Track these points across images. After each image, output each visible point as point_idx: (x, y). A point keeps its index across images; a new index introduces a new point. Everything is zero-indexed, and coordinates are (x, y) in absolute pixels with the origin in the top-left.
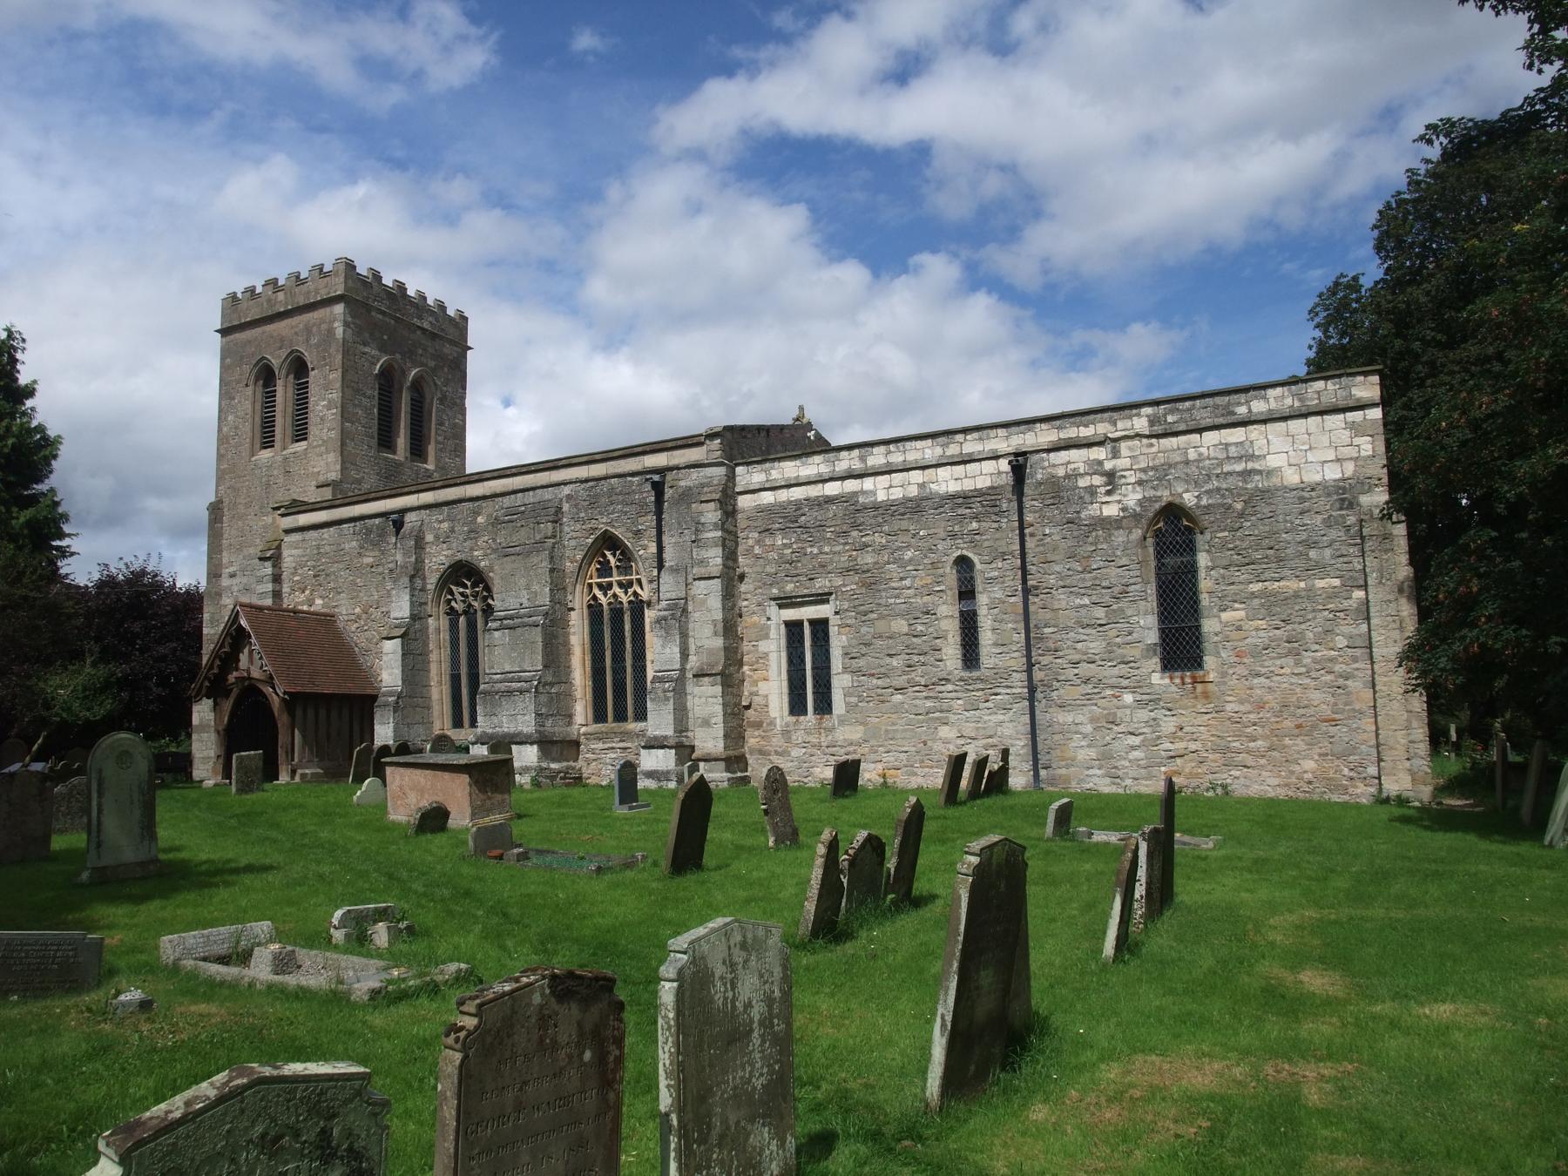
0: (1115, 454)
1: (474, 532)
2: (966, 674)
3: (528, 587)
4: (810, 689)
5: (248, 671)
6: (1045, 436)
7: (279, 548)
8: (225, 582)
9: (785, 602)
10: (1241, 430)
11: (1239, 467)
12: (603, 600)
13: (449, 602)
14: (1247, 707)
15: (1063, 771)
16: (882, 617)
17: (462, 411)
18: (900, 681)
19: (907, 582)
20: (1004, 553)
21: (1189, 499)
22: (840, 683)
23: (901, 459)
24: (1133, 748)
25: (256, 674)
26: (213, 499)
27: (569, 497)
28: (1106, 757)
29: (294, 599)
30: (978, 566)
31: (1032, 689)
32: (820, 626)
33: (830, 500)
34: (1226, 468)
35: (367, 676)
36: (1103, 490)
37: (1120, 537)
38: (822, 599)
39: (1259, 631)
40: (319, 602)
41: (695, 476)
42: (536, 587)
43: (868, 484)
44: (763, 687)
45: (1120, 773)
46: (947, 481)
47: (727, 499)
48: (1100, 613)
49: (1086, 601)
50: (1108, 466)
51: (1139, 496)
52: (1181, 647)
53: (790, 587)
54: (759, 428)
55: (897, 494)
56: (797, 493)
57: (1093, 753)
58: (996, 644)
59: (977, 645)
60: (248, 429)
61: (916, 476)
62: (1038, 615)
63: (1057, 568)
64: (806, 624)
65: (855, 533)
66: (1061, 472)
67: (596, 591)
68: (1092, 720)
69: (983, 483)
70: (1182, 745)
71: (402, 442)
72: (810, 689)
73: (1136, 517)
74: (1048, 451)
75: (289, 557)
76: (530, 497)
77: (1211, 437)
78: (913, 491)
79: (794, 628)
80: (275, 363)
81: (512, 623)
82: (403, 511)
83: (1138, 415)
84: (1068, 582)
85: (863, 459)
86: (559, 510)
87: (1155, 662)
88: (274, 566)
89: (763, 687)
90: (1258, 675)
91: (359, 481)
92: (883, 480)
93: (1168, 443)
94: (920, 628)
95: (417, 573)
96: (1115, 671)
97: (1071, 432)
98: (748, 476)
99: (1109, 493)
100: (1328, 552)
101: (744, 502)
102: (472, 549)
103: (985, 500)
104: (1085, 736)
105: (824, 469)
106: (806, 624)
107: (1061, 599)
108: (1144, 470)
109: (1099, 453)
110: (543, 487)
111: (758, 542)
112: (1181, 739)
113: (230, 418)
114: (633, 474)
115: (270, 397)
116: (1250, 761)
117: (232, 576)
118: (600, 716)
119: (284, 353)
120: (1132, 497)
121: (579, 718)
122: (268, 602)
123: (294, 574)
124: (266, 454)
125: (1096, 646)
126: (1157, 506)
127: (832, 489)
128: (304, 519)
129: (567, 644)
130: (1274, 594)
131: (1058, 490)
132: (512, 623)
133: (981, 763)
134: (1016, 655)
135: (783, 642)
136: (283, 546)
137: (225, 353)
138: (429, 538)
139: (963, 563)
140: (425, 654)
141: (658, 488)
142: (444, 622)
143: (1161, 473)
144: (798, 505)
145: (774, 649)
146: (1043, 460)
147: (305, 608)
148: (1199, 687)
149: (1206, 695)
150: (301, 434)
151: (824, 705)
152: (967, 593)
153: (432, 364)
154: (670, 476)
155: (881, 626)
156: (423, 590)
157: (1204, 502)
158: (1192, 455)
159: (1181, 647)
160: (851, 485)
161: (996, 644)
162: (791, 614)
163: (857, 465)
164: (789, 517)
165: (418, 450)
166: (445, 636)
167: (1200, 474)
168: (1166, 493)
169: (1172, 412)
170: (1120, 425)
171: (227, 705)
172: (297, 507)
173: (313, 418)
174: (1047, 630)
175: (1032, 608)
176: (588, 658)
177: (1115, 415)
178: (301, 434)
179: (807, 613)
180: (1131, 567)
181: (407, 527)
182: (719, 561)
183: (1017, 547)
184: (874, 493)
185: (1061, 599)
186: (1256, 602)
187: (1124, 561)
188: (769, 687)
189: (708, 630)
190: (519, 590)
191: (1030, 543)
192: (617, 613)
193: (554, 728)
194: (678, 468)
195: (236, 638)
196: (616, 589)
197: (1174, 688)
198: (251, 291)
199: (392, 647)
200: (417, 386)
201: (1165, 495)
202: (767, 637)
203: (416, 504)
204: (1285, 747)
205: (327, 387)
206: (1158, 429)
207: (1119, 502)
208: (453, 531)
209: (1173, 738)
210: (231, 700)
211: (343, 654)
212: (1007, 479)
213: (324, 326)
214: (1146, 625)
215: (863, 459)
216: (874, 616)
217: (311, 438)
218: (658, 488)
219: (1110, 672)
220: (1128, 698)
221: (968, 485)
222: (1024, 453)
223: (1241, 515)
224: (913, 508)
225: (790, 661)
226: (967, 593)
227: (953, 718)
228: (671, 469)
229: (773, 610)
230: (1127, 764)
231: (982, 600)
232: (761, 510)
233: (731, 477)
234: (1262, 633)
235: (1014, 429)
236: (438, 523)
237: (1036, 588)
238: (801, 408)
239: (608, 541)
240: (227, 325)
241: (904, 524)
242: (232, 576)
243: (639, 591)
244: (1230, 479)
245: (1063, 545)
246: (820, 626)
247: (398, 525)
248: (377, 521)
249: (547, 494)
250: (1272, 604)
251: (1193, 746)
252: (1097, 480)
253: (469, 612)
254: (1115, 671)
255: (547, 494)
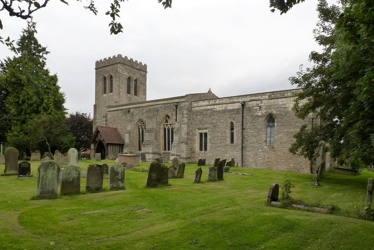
0: (261, 103)
1: (143, 114)
2: (231, 144)
3: (152, 124)
4: (203, 146)
5: (100, 139)
8: (97, 121)
9: (199, 129)
12: (166, 127)
13: (138, 126)
15: (247, 164)
16: (217, 133)
17: (146, 86)
18: (219, 145)
19: (221, 126)
20: (239, 121)
21: (274, 112)
22: (209, 145)
23: (222, 102)
24: (260, 160)
25: (101, 139)
26: (94, 104)
28: (255, 161)
29: (110, 125)
31: (242, 148)
32: (206, 134)
33: (209, 110)
34: (282, 106)
35: (124, 141)
36: (258, 110)
37: (260, 119)
38: (206, 129)
41: (183, 104)
42: (153, 125)
43: (216, 107)
45: (257, 164)
48: (256, 134)
49: (254, 132)
50: (260, 105)
51: (265, 111)
53: (200, 126)
55: (221, 109)
56: (203, 108)
57: (253, 160)
58: (237, 139)
59: (233, 139)
60: (101, 90)
62: (245, 134)
63: (249, 125)
64: (203, 135)
65: (213, 116)
66: (251, 106)
67: (165, 125)
68: (253, 154)
69: (236, 107)
70: (269, 160)
71: (132, 91)
72: (203, 146)
73: (264, 115)
74: (249, 101)
75: (109, 116)
76: (153, 107)
78: (224, 108)
79: (201, 134)
82: (130, 109)
83: (266, 95)
84: (251, 127)
85: (215, 102)
86: (158, 110)
88: (106, 118)
90: (284, 147)
91: (123, 101)
93: (272, 101)
94: (223, 135)
96: (258, 145)
97: (253, 98)
99: (259, 110)
100: (300, 124)
102: (143, 117)
103: (236, 111)
104: (252, 157)
106: (203, 135)
107: (249, 131)
108: (267, 106)
109: (259, 102)
110: (156, 105)
111: (195, 117)
112: (269, 159)
113: (98, 87)
114: (172, 103)
115: (105, 83)
116: (281, 164)
117: (99, 119)
119: (108, 74)
120: (264, 111)
122: (105, 126)
123: (110, 120)
124: (105, 95)
125: (255, 140)
126: (268, 113)
127: (209, 107)
128: (111, 109)
130: (288, 132)
131: (250, 109)
132: (149, 131)
134: (240, 141)
135: (199, 137)
136: (107, 114)
137: (97, 73)
139: (232, 123)
141: (176, 106)
143: (269, 107)
144: (203, 110)
145: (197, 138)
146: (248, 103)
147: (112, 127)
148: (273, 149)
149: (274, 151)
150: (111, 91)
151: (206, 149)
152: (232, 129)
153: (139, 76)
154: (179, 104)
155: (216, 135)
157: (277, 113)
158: (276, 103)
160: (213, 107)
161: (237, 139)
162: (201, 131)
163: (214, 103)
164: (201, 113)
167: (278, 107)
168: (270, 111)
169: (273, 94)
170: (263, 97)
171: (96, 145)
172: (110, 107)
173: (114, 88)
174: (246, 137)
175: (244, 132)
177: (262, 94)
178: (111, 91)
181: (130, 112)
183: (241, 120)
184: (216, 108)
185: (249, 131)
186: (285, 133)
188: (197, 146)
189: (184, 134)
191: (244, 120)
194: (180, 102)
195: (98, 132)
196: (169, 125)
197: (268, 149)
198: (101, 60)
200: (136, 81)
201: (270, 111)
202: (196, 136)
203: (132, 107)
204: (288, 161)
205: (116, 82)
206: (270, 98)
207: (261, 112)
208: (139, 113)
209: (268, 158)
210: (97, 144)
211: (120, 137)
212: (241, 107)
213: (116, 69)
215: (215, 102)
216: (215, 132)
217: (113, 92)
218: (176, 106)
219: (257, 145)
220: (260, 150)
221: (234, 108)
222: (244, 102)
224: (224, 111)
225: (200, 140)
227: (228, 152)
228: (179, 102)
229: (197, 130)
230: (259, 163)
231: (235, 130)
234: (285, 139)
235: (242, 97)
236: (137, 111)
237: (245, 128)
238: (210, 89)
240: (96, 68)
241: (222, 115)
242: (99, 119)
243: (173, 126)
244: (282, 108)
245: (250, 120)
247: (129, 111)
248: (125, 110)
249: (157, 106)
251: (271, 160)
252: (258, 108)
254: (258, 145)
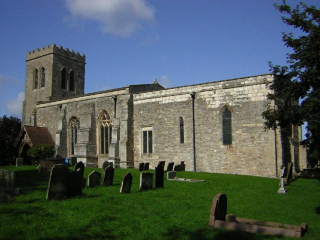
0: (215, 93)
6: (200, 88)
7: (36, 112)
8: (26, 120)
10: (242, 88)
11: (242, 97)
14: (241, 154)
21: (230, 104)
27: (97, 101)
29: (39, 124)
30: (184, 119)
32: (150, 132)
39: (245, 136)
40: (44, 125)
43: (161, 99)
44: (138, 146)
46: (178, 99)
47: (130, 104)
50: (213, 96)
52: (227, 139)
54: (141, 85)
55: (167, 102)
56: (146, 101)
61: (172, 97)
69: (185, 100)
76: (89, 101)
77: (235, 89)
80: (38, 68)
81: (83, 131)
82: (61, 105)
87: (221, 143)
89: (138, 146)
92: (165, 98)
95: (64, 118)
98: (136, 97)
101: (135, 103)
103: (187, 102)
105: (152, 95)
109: (211, 92)
118: (103, 152)
121: (98, 153)
124: (35, 90)
127: (153, 100)
129: (95, 136)
132: (83, 131)
133: (171, 165)
138: (67, 110)
140: (66, 138)
141: (115, 100)
142: (70, 130)
144: (146, 104)
148: (231, 149)
149: (232, 150)
152: (182, 125)
156: (66, 122)
159: (227, 139)
162: (144, 129)
165: (72, 89)
166: (70, 133)
176: (100, 138)
179: (148, 129)
180: (217, 120)
182: (127, 117)
187: (216, 118)
188: (139, 146)
190: (85, 124)
192: (107, 128)
193: (91, 155)
196: (107, 123)
199: (58, 136)
200: (72, 73)
214: (219, 133)
218: (115, 100)
219: (212, 144)
220: (215, 151)
223: (241, 108)
226: (182, 125)
231: (185, 127)
232: (138, 105)
233: (132, 97)
239: (105, 111)
246: (150, 132)
247: (61, 107)
250: (249, 130)
253: (75, 127)
255: (93, 100)
